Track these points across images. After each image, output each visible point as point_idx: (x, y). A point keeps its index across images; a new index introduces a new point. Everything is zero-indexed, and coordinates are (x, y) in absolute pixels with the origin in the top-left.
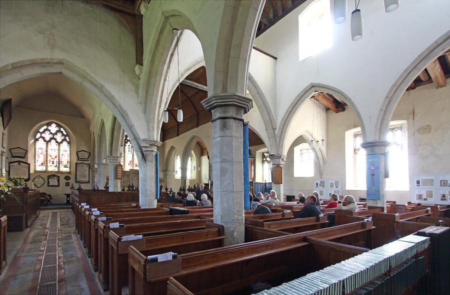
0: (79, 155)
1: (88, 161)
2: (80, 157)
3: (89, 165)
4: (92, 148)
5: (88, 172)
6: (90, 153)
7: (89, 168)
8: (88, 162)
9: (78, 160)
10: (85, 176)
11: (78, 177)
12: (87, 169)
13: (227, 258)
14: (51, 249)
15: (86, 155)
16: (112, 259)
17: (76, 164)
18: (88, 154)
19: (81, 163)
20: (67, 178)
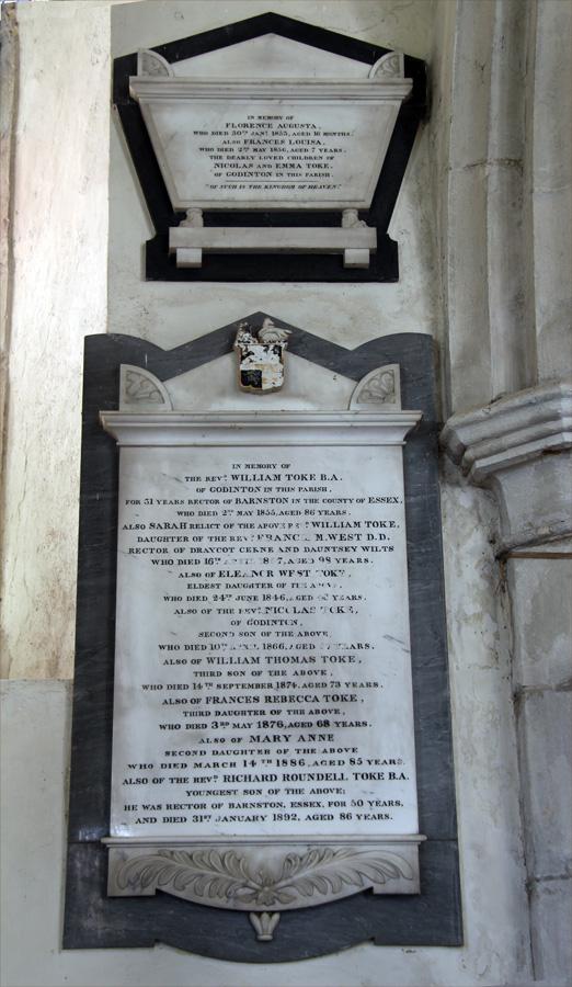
0: (177, 125)
1: (383, 265)
2: (192, 183)
3: (416, 364)
4: (441, 327)
5: (383, 584)
6: (418, 71)
7: (431, 452)
8: (393, 308)
9: (160, 263)
10: (316, 713)
11: (138, 732)
12: (374, 476)
13: (456, 928)
14: (467, 697)
15: (344, 125)
16: (229, 422)
17: (107, 364)
18: (384, 90)
19: (224, 341)
20: (301, 859)
